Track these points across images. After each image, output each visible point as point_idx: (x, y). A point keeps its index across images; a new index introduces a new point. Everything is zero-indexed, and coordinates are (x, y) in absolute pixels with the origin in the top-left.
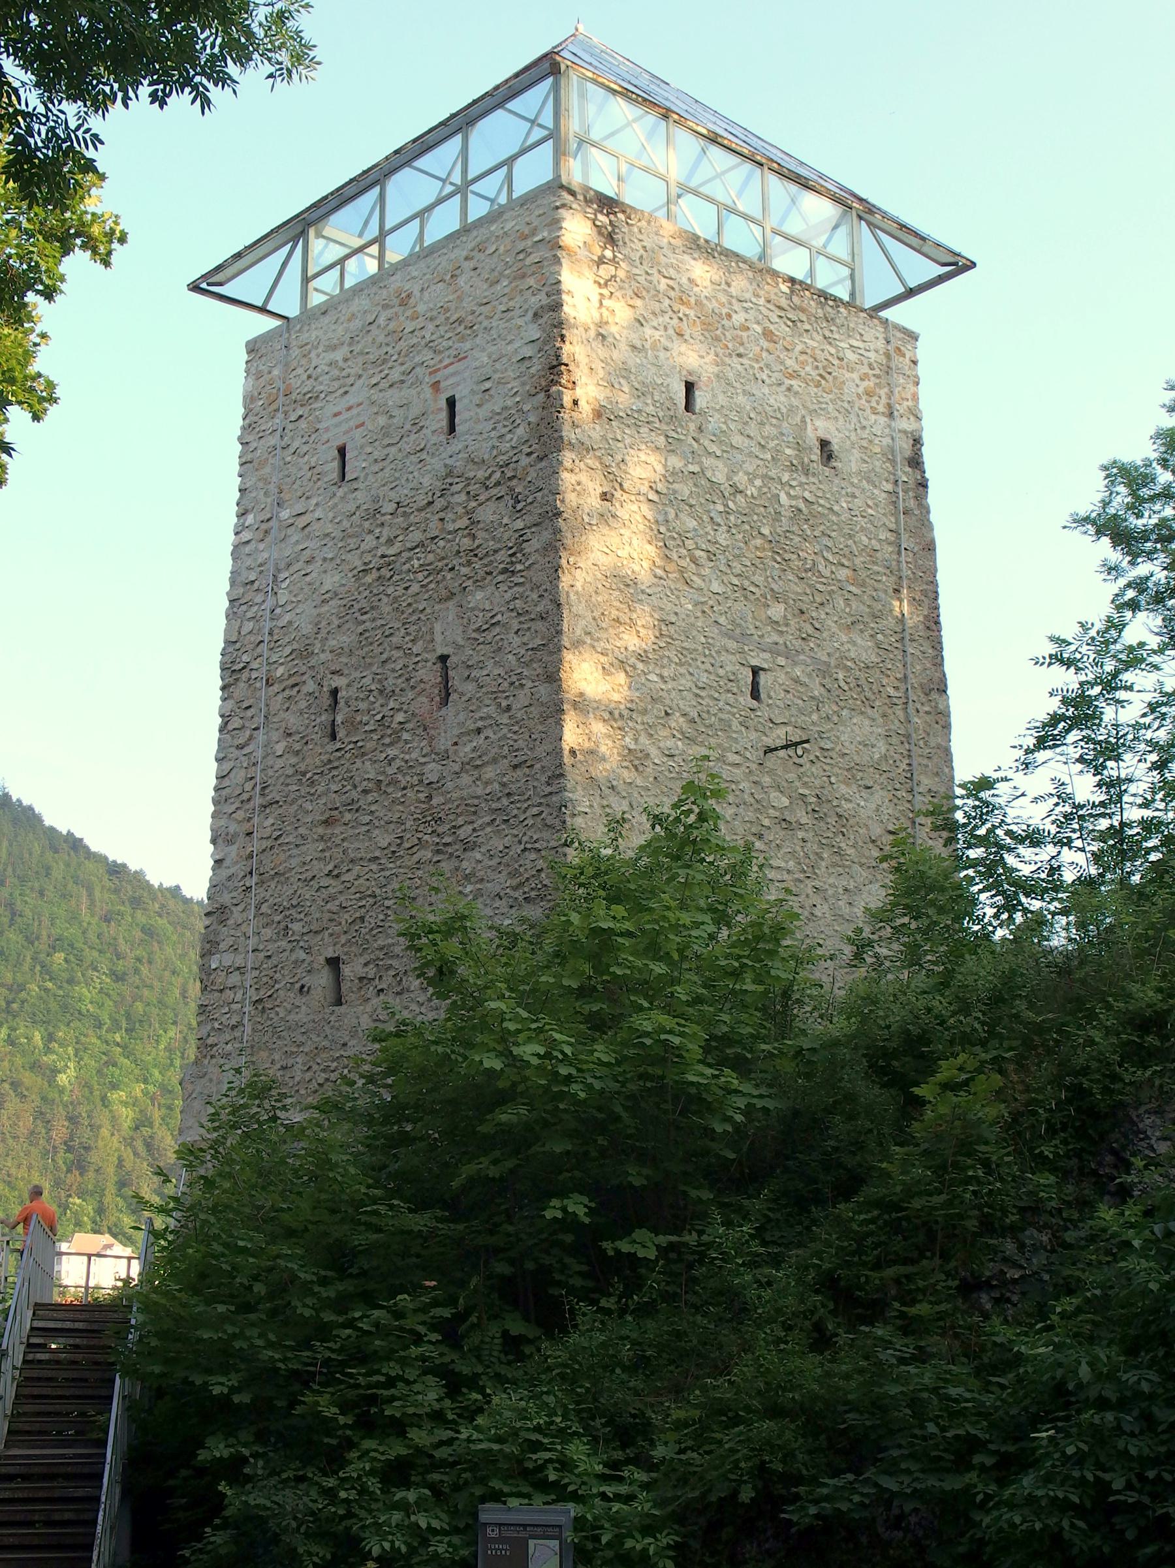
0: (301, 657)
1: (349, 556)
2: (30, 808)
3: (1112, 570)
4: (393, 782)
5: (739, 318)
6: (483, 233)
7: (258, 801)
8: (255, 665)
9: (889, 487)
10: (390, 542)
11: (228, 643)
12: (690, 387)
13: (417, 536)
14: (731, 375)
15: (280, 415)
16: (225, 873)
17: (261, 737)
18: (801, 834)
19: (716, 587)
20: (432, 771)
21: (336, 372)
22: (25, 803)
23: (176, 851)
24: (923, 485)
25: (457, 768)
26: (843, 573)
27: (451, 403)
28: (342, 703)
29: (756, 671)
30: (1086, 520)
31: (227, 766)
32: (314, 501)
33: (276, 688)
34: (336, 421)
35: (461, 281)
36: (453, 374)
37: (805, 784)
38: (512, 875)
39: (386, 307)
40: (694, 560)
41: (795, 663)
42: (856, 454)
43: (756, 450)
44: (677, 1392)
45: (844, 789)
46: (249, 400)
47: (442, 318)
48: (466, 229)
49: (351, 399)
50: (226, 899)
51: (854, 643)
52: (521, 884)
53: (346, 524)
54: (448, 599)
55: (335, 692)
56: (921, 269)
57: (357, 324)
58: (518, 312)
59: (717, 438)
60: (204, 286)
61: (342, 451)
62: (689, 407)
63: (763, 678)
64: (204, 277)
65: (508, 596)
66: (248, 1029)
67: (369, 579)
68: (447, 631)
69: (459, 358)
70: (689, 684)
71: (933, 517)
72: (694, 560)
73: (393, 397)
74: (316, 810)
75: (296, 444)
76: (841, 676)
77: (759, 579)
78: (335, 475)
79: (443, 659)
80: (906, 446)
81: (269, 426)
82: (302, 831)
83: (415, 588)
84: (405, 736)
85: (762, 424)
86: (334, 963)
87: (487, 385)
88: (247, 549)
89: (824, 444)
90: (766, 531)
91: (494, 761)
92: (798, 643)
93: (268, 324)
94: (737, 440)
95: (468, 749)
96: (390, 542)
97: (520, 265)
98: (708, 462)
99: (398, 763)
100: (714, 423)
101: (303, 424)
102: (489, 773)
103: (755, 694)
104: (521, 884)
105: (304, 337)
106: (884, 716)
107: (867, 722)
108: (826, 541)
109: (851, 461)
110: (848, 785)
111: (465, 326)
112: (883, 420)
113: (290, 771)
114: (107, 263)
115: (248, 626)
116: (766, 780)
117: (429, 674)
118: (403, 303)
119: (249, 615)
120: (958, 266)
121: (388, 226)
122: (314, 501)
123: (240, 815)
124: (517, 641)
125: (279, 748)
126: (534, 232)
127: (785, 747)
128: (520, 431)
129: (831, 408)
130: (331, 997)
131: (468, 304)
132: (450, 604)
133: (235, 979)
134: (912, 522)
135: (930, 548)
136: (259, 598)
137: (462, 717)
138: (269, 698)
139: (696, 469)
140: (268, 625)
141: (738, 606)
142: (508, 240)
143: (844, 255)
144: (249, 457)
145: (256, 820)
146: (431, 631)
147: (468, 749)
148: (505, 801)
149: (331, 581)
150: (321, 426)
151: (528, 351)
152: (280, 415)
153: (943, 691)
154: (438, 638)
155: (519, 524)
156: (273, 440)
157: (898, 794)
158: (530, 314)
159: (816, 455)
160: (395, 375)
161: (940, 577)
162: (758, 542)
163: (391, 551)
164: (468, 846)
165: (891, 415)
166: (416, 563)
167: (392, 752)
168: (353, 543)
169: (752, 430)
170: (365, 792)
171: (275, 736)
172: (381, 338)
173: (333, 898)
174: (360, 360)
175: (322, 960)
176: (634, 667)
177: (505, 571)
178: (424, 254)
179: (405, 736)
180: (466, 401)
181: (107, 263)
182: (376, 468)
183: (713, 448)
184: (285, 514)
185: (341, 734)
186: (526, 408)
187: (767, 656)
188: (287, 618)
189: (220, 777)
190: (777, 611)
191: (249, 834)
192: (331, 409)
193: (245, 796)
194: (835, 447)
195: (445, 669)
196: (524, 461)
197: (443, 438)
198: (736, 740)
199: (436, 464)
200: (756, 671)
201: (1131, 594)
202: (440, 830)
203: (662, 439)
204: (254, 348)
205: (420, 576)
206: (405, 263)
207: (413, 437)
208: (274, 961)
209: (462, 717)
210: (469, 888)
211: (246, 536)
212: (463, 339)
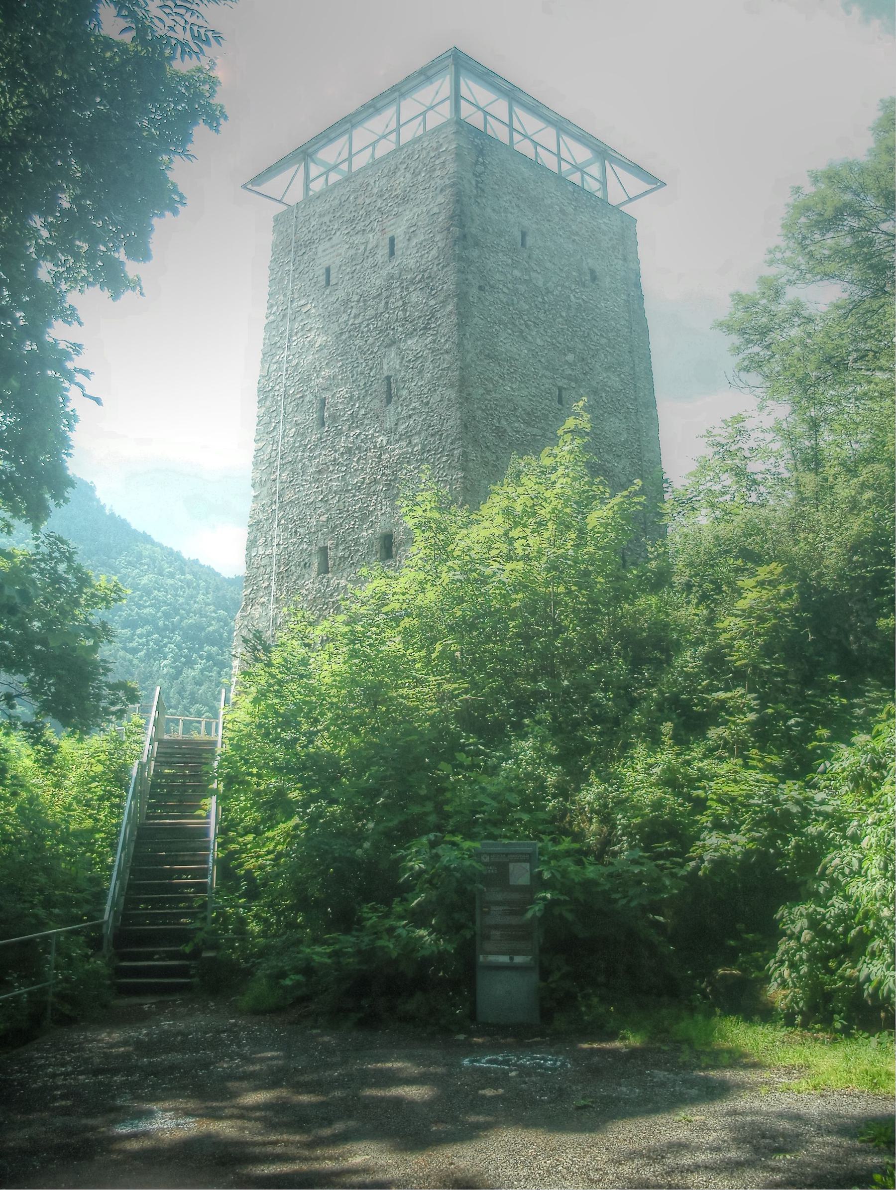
1: (332, 325)
2: (125, 520)
3: (737, 350)
9: (624, 297)
12: (524, 235)
14: (544, 230)
20: (382, 439)
22: (122, 517)
25: (397, 437)
26: (604, 341)
27: (392, 240)
28: (327, 406)
29: (560, 389)
30: (720, 325)
31: (261, 445)
36: (393, 225)
39: (354, 191)
40: (527, 326)
41: (580, 387)
43: (558, 271)
48: (400, 149)
56: (635, 185)
60: (249, 186)
61: (328, 270)
62: (523, 245)
63: (564, 394)
67: (344, 337)
70: (526, 393)
72: (527, 326)
73: (358, 239)
76: (604, 395)
77: (561, 339)
79: (388, 378)
83: (371, 340)
89: (592, 271)
90: (564, 314)
92: (582, 376)
94: (548, 265)
97: (431, 164)
98: (533, 275)
101: (306, 257)
103: (560, 401)
106: (625, 418)
107: (617, 421)
108: (594, 322)
110: (608, 454)
112: (621, 262)
114: (217, 131)
119: (274, 361)
121: (354, 152)
135: (646, 330)
138: (285, 406)
139: (527, 277)
140: (286, 366)
146: (381, 363)
154: (385, 367)
155: (432, 302)
157: (634, 460)
162: (560, 319)
165: (625, 259)
176: (498, 382)
177: (425, 328)
178: (375, 163)
179: (366, 422)
180: (401, 238)
181: (217, 131)
183: (535, 268)
187: (566, 381)
193: (272, 460)
198: (551, 425)
199: (384, 272)
200: (560, 389)
201: (746, 363)
202: (387, 472)
203: (510, 261)
204: (276, 219)
205: (374, 334)
206: (364, 169)
207: (370, 259)
211: (272, 318)
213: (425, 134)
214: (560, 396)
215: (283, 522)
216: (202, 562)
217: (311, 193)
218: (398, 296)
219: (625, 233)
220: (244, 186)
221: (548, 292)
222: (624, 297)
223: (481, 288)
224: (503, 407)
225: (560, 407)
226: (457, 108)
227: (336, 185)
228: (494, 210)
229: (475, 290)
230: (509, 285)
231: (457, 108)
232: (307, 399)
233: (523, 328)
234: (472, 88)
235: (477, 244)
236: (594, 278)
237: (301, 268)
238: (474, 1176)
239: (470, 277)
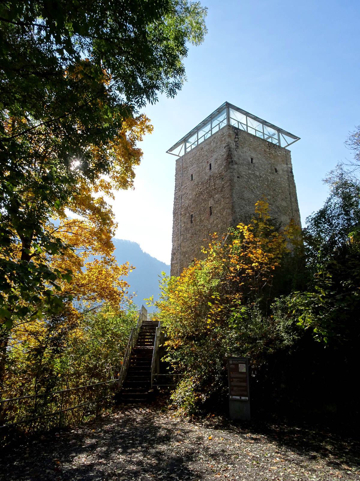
12: (252, 159)
16: (174, 247)
23: (168, 262)
27: (210, 165)
34: (191, 171)
40: (254, 188)
42: (281, 171)
44: (124, 320)
49: (193, 167)
56: (290, 140)
57: (194, 154)
61: (192, 175)
62: (252, 162)
69: (212, 157)
72: (254, 188)
77: (265, 192)
78: (191, 179)
79: (210, 207)
80: (290, 170)
89: (276, 169)
93: (179, 157)
94: (260, 168)
98: (256, 172)
100: (256, 165)
101: (185, 172)
111: (213, 151)
115: (177, 206)
117: (208, 210)
125: (183, 226)
135: (295, 187)
143: (277, 138)
149: (190, 197)
151: (223, 154)
154: (209, 204)
155: (223, 183)
159: (274, 171)
169: (263, 166)
183: (256, 169)
184: (183, 187)
190: (269, 197)
199: (208, 175)
204: (177, 161)
211: (176, 191)
219: (287, 155)
220: (167, 152)
221: (261, 177)
226: (229, 121)
229: (236, 178)
235: (236, 163)
239: (234, 174)
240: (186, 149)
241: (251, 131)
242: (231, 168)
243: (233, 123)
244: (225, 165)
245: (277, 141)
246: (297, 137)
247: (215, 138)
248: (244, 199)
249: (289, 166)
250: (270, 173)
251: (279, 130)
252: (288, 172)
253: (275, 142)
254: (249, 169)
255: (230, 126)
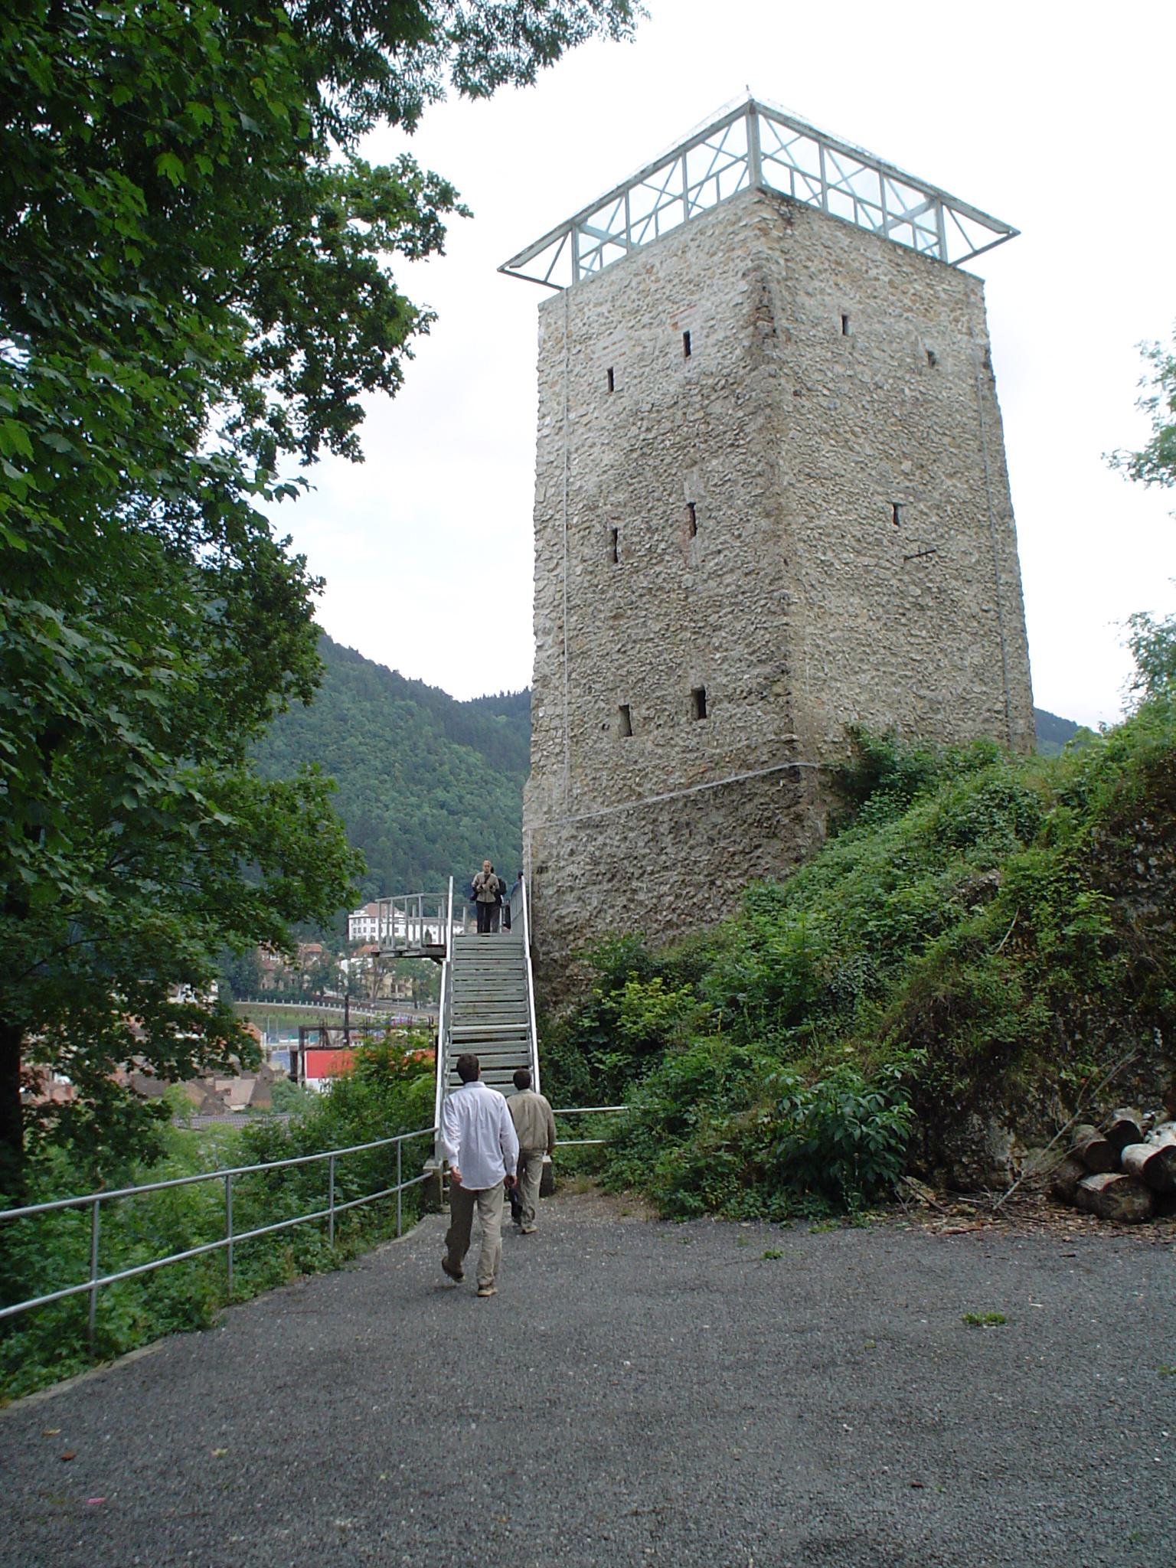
0: (591, 509)
4: (661, 588)
5: (873, 272)
6: (702, 222)
7: (564, 605)
8: (557, 516)
9: (972, 382)
10: (648, 430)
11: (537, 502)
12: (844, 318)
13: (668, 425)
14: (869, 310)
15: (564, 351)
17: (564, 563)
18: (929, 613)
19: (869, 451)
20: (688, 579)
21: (603, 321)
24: (992, 380)
25: (705, 577)
26: (946, 440)
27: (687, 336)
28: (620, 538)
29: (896, 506)
31: (542, 584)
32: (592, 406)
33: (574, 530)
34: (609, 350)
35: (689, 255)
37: (931, 581)
38: (748, 646)
39: (636, 275)
40: (854, 433)
45: (954, 583)
46: (542, 342)
47: (676, 281)
49: (615, 337)
50: (547, 670)
51: (955, 486)
52: (754, 652)
53: (616, 420)
54: (692, 466)
55: (615, 531)
56: (983, 236)
57: (615, 288)
58: (731, 273)
59: (865, 351)
60: (507, 268)
61: (611, 372)
63: (900, 512)
64: (508, 263)
65: (735, 461)
66: (568, 755)
67: (635, 455)
68: (692, 487)
69: (690, 306)
71: (1000, 402)
72: (854, 433)
73: (645, 334)
74: (606, 610)
75: (577, 370)
79: (691, 505)
80: (981, 354)
81: (558, 358)
82: (598, 623)
83: (668, 460)
84: (667, 558)
85: (891, 342)
86: (625, 709)
87: (712, 322)
88: (547, 440)
89: (930, 354)
91: (732, 571)
94: (876, 353)
95: (712, 564)
96: (648, 430)
99: (663, 575)
101: (582, 356)
102: (728, 579)
104: (754, 652)
105: (579, 299)
108: (934, 418)
109: (948, 365)
112: (966, 338)
113: (586, 585)
116: (906, 578)
118: (649, 272)
120: (1010, 233)
122: (592, 406)
123: (554, 615)
124: (743, 491)
126: (740, 219)
127: (919, 556)
128: (738, 352)
129: (933, 331)
130: (624, 731)
131: (695, 270)
132: (695, 469)
133: (556, 722)
134: (988, 404)
135: (999, 422)
136: (557, 473)
137: (706, 543)
141: (883, 463)
142: (721, 227)
144: (544, 379)
145: (565, 618)
147: (712, 564)
148: (740, 597)
149: (609, 458)
150: (595, 356)
152: (564, 351)
153: (1011, 516)
154: (687, 492)
155: (741, 414)
156: (563, 367)
158: (740, 275)
160: (646, 320)
161: (1006, 441)
162: (893, 420)
163: (650, 436)
164: (717, 629)
165: (970, 334)
166: (668, 443)
167: (658, 569)
168: (622, 432)
170: (641, 596)
171: (575, 562)
172: (634, 296)
173: (622, 666)
174: (620, 311)
175: (616, 707)
177: (732, 445)
179: (667, 558)
182: (636, 381)
183: (862, 359)
184: (572, 416)
185: (621, 559)
186: (741, 336)
188: (578, 484)
189: (538, 592)
191: (560, 628)
192: (602, 344)
194: (937, 356)
195: (693, 512)
196: (742, 372)
197: (682, 359)
199: (679, 376)
200: (896, 506)
202: (696, 618)
204: (543, 308)
208: (583, 708)
209: (706, 543)
210: (718, 656)
211: (545, 432)
212: (692, 293)
213: (720, 204)
214: (895, 514)
215: (574, 676)
216: (428, 682)
217: (582, 273)
218: (697, 406)
219: (969, 294)
220: (502, 270)
222: (972, 382)
223: (796, 394)
224: (829, 535)
225: (896, 527)
226: (755, 167)
227: (615, 265)
228: (808, 294)
230: (830, 385)
231: (755, 167)
232: (594, 531)
233: (848, 436)
234: (770, 136)
236: (932, 361)
237: (577, 370)
238: (827, 1216)
239: (783, 381)
240: (576, 260)
241: (839, 206)
242: (770, 360)
243: (776, 178)
244: (746, 343)
245: (934, 239)
246: (1008, 227)
247: (702, 232)
248: (816, 478)
249: (981, 341)
250: (912, 371)
251: (938, 199)
252: (973, 365)
253: (925, 243)
254: (837, 358)
255: (764, 193)
